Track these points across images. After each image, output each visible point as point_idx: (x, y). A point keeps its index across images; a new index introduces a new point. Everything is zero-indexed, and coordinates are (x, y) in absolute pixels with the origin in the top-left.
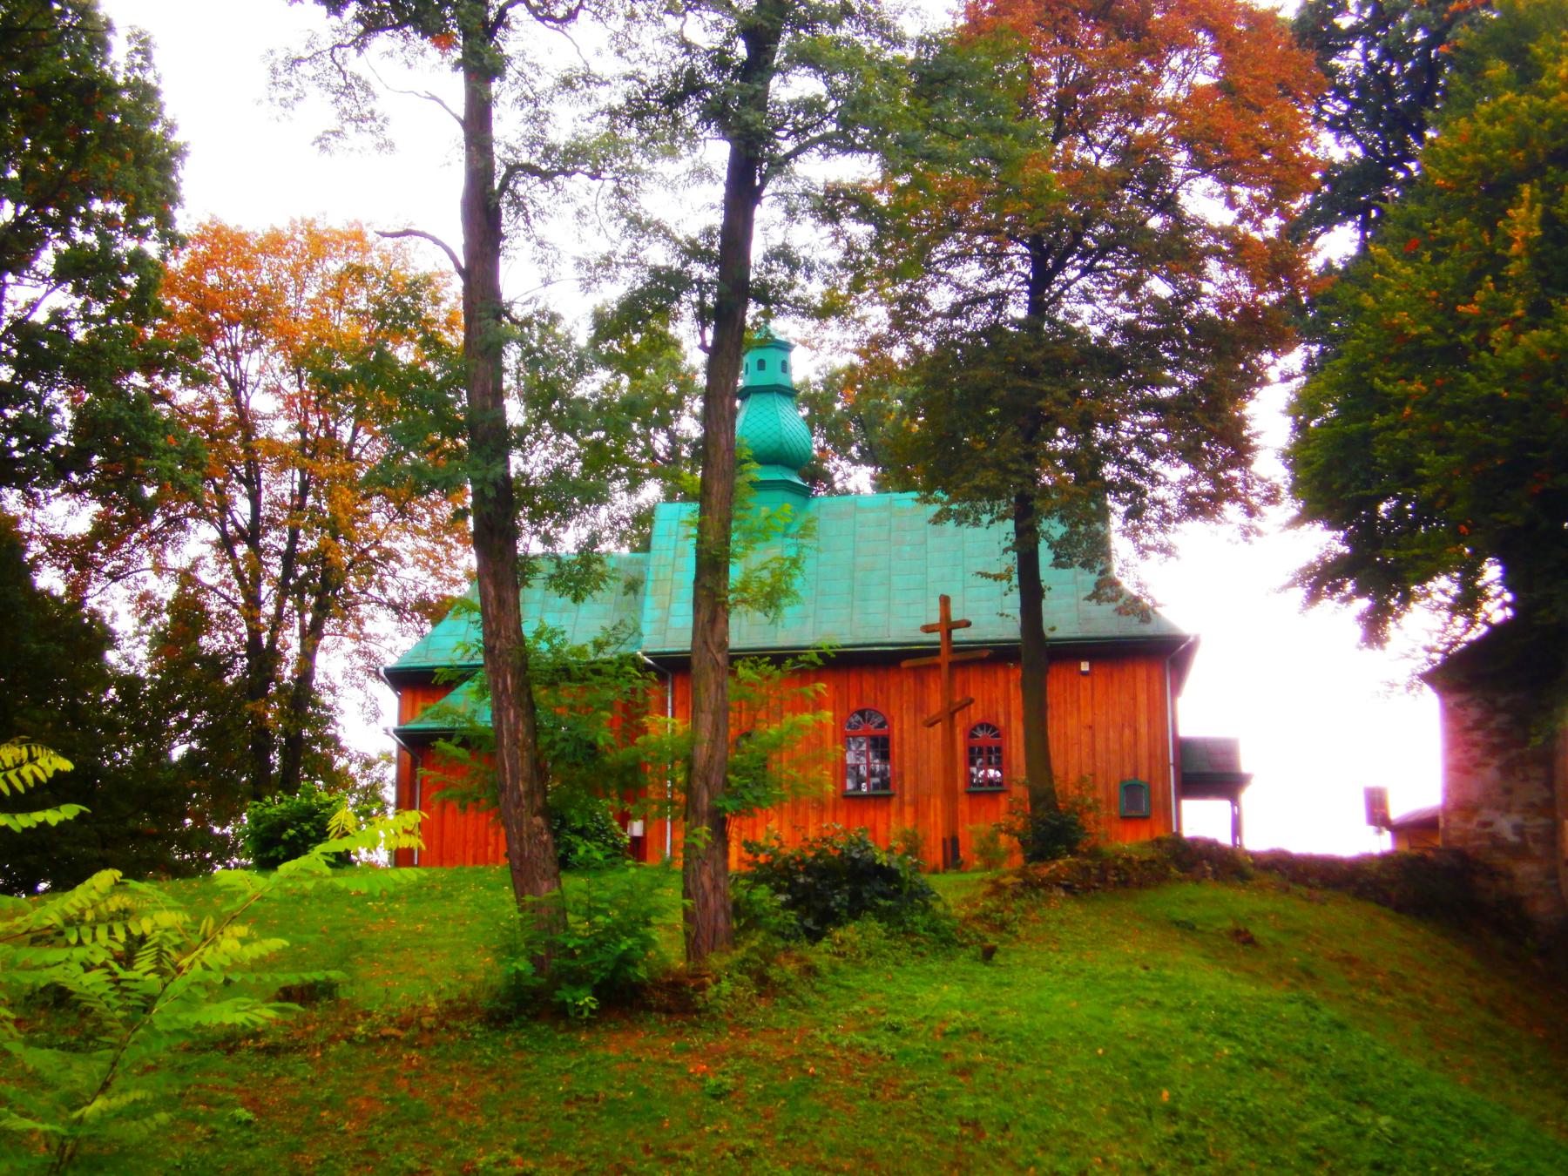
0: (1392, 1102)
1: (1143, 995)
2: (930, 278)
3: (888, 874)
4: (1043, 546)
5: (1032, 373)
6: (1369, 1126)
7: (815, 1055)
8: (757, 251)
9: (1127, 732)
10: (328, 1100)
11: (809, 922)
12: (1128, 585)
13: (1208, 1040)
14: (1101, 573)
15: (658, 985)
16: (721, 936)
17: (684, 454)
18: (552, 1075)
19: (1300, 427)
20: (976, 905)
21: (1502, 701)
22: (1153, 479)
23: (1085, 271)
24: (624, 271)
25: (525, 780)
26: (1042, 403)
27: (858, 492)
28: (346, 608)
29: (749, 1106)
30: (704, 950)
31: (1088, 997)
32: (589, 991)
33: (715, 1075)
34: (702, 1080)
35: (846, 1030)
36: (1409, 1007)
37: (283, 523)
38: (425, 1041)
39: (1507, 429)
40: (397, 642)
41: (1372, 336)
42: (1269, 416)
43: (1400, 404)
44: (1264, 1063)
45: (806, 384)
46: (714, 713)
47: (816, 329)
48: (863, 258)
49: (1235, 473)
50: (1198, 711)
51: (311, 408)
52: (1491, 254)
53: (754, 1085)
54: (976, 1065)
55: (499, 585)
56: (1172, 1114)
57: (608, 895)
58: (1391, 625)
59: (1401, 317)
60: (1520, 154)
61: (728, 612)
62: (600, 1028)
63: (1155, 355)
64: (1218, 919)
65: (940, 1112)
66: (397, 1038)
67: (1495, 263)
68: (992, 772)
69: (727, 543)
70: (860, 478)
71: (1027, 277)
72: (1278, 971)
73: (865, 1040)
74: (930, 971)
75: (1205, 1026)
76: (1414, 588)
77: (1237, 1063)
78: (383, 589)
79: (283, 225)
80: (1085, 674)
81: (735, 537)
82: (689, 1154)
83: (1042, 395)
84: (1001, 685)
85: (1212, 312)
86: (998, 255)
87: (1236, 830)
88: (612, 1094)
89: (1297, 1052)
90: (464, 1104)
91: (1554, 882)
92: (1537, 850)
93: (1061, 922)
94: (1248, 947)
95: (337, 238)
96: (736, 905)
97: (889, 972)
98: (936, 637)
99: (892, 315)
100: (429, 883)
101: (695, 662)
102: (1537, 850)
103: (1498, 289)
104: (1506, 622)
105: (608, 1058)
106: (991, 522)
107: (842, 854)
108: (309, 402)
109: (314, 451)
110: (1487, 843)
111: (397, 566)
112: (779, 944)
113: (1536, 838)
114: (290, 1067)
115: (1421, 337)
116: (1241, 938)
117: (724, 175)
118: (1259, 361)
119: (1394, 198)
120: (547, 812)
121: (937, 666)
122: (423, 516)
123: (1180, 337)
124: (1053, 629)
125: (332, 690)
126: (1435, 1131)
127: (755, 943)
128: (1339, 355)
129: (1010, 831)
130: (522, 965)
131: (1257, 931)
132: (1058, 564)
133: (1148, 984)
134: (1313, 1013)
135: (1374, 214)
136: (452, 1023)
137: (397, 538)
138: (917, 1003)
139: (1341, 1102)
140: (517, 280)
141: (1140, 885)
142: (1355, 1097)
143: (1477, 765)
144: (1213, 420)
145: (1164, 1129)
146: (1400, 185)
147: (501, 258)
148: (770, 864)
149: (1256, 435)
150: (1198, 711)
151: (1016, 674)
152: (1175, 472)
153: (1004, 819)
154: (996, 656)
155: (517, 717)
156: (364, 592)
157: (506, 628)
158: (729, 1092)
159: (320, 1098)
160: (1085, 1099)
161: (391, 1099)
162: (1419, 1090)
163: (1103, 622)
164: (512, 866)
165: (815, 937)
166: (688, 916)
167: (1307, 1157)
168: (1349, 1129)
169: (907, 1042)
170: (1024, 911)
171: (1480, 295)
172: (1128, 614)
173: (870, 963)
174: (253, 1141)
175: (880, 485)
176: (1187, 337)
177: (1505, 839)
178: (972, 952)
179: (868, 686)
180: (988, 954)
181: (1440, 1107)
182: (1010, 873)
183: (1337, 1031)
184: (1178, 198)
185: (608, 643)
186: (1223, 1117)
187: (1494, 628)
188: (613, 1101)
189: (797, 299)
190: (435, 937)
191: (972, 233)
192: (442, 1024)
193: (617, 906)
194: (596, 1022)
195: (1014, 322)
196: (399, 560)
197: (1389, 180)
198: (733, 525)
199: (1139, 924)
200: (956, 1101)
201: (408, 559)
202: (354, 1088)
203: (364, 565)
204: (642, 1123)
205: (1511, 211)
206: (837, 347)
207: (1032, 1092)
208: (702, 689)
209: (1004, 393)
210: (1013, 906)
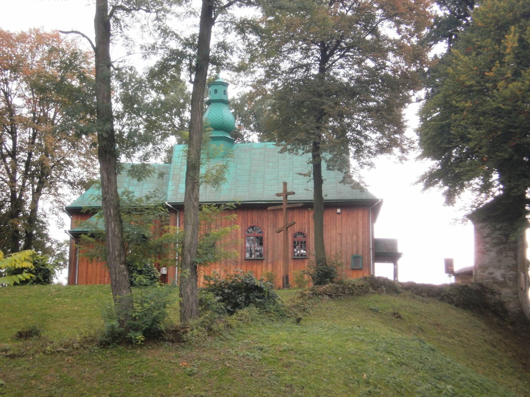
0: (452, 380)
2: (281, 58)
3: (259, 289)
5: (320, 96)
6: (443, 389)
7: (229, 359)
8: (213, 42)
9: (354, 236)
10: (34, 376)
11: (229, 308)
12: (355, 178)
14: (345, 173)
15: (168, 331)
16: (194, 312)
17: (186, 126)
18: (125, 367)
19: (422, 120)
20: (294, 302)
21: (498, 226)
22: (366, 138)
23: (341, 56)
24: (160, 51)
25: (118, 250)
26: (323, 107)
27: (253, 142)
28: (51, 183)
29: (203, 379)
30: (187, 318)
31: (336, 338)
32: (142, 334)
33: (190, 366)
34: (185, 369)
35: (242, 349)
36: (460, 343)
37: (26, 149)
38: (75, 353)
39: (503, 121)
40: (70, 197)
41: (451, 84)
42: (412, 115)
43: (462, 111)
44: (403, 364)
45: (233, 99)
47: (236, 77)
48: (254, 48)
49: (397, 136)
50: (382, 229)
51: (38, 103)
53: (205, 371)
54: (292, 363)
55: (108, 173)
56: (367, 383)
57: (149, 296)
58: (456, 197)
59: (463, 78)
60: (511, 14)
61: (199, 186)
62: (145, 347)
63: (367, 90)
64: (387, 308)
65: (278, 382)
66: (63, 352)
67: (500, 56)
68: (302, 251)
69: (199, 159)
70: (254, 137)
71: (319, 58)
73: (249, 353)
74: (276, 327)
75: (381, 349)
76: (466, 182)
77: (393, 363)
78: (66, 176)
79: (26, 30)
80: (339, 213)
81: (202, 156)
83: (323, 104)
84: (306, 217)
85: (390, 73)
86: (308, 49)
87: (396, 275)
88: (149, 374)
89: (416, 360)
90: (89, 378)
91: (516, 296)
92: (510, 284)
93: (327, 309)
94: (399, 319)
95: (48, 36)
96: (201, 300)
97: (259, 327)
98: (281, 198)
99: (267, 72)
101: (186, 205)
102: (510, 284)
103: (501, 66)
104: (500, 195)
105: (148, 360)
106: (303, 153)
107: (243, 281)
108: (36, 101)
109: (38, 121)
110: (491, 281)
111: (72, 167)
112: (217, 316)
113: (510, 279)
114: (20, 363)
115: (471, 86)
116: (396, 316)
117: (200, 14)
118: (408, 94)
119: (462, 31)
120: (126, 263)
121: (281, 209)
122: (82, 148)
123: (378, 83)
124: (326, 196)
125: (45, 216)
126: (469, 391)
127: (207, 315)
128: (439, 92)
129: (308, 273)
130: (115, 323)
131: (402, 313)
132: (328, 168)
134: (423, 345)
135: (453, 37)
136: (86, 346)
137: (72, 156)
138: (270, 339)
139: (433, 379)
140: (116, 52)
142: (438, 378)
143: (487, 251)
144: (389, 115)
145: (364, 389)
146: (464, 26)
147: (111, 44)
148: (215, 285)
149: (406, 121)
150: (382, 229)
151: (311, 214)
152: (374, 136)
153: (306, 269)
154: (306, 206)
155: (115, 225)
156: (58, 177)
157: (111, 191)
158: (195, 373)
159: (31, 375)
160: (334, 377)
161: (60, 376)
162: (463, 375)
163: (346, 193)
164: (112, 285)
165: (231, 313)
166: (181, 304)
168: (435, 390)
169: (265, 354)
170: (313, 304)
171: (494, 69)
172: (356, 189)
173: (252, 323)
174: (3, 392)
175: (261, 140)
176: (380, 83)
177: (498, 279)
178: (293, 320)
179: (254, 217)
180: (299, 320)
181: (471, 382)
182: (308, 289)
183: (432, 352)
184: (378, 28)
185: (151, 197)
187: (496, 198)
188: (149, 377)
189: (228, 64)
190: (82, 312)
191: (297, 40)
192: (82, 346)
193: (153, 300)
194: (143, 345)
195: (313, 75)
196: (73, 165)
197: (460, 24)
198: (202, 151)
199: (357, 310)
200: (284, 377)
201: (76, 165)
202: (45, 372)
203: (59, 166)
204: (160, 385)
205: (506, 36)
206: (245, 84)
207: (313, 374)
208: (188, 216)
209: (308, 103)
210: (308, 302)
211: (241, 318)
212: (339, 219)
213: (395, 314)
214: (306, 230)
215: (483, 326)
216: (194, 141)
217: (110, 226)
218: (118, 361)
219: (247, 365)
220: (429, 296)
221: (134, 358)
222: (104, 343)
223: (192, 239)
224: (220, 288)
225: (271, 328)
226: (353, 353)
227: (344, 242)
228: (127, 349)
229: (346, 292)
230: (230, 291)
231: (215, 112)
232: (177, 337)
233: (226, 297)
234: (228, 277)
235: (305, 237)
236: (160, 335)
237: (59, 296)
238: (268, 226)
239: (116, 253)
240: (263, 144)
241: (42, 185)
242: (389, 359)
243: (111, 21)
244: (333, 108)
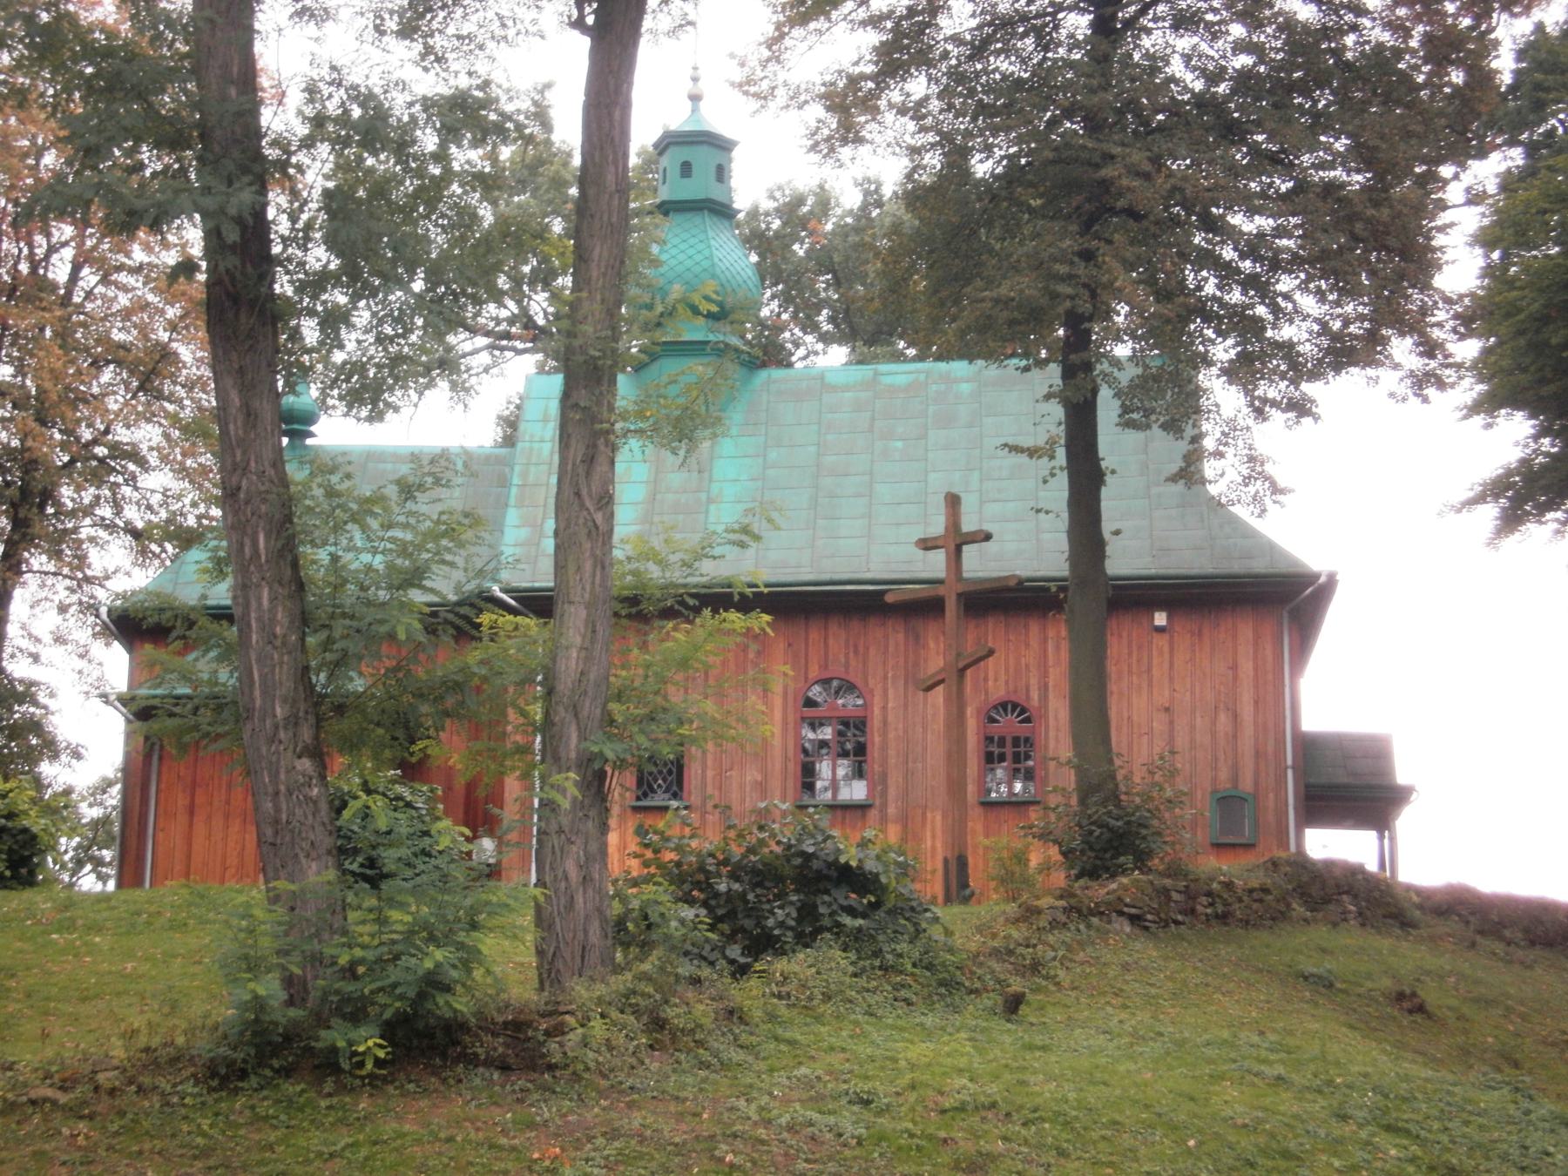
1: (1256, 1067)
4: (1105, 394)
7: (735, 1136)
9: (1223, 718)
13: (1363, 1134)
18: (307, 1162)
25: (284, 701)
26: (1108, 172)
31: (1171, 1068)
32: (377, 1031)
35: (786, 1101)
40: (122, 572)
46: (588, 606)
50: (1330, 695)
54: (992, 1157)
61: (614, 449)
62: (390, 1089)
64: (1369, 976)
66: (54, 1103)
72: (1466, 1055)
73: (815, 1116)
74: (921, 1024)
75: (1360, 1114)
89: (1505, 1158)
93: (1126, 967)
94: (1418, 1018)
97: (856, 1023)
98: (935, 564)
100: (153, 909)
105: (402, 1135)
112: (686, 969)
116: (1406, 1005)
127: (646, 966)
131: (1430, 995)
133: (1264, 1053)
134: (1526, 1104)
136: (146, 1080)
141: (1246, 923)
150: (1330, 695)
163: (1186, 556)
165: (740, 971)
166: (541, 920)
170: (1069, 949)
173: (828, 1009)
178: (989, 1003)
179: (834, 643)
180: (1013, 1005)
185: (421, 487)
194: (385, 1080)
196: (142, 463)
199: (1246, 974)
201: (153, 459)
211: (784, 989)
212: (1161, 653)
213: (1401, 997)
214: (1035, 695)
216: (594, 265)
217: (254, 604)
218: (279, 1142)
219: (807, 1161)
220: (1533, 943)
221: (344, 1130)
222: (223, 1071)
223: (587, 659)
224: (701, 877)
225: (902, 1029)
226: (1245, 1126)
228: (319, 1093)
229: (1199, 908)
230: (736, 886)
231: (683, 246)
232: (520, 1048)
233: (720, 912)
234: (732, 834)
235: (1028, 720)
236: (456, 1043)
237: (68, 926)
238: (885, 678)
239: (278, 711)
240: (866, 371)
241: (24, 535)
242: (1393, 1152)
244: (1147, 176)
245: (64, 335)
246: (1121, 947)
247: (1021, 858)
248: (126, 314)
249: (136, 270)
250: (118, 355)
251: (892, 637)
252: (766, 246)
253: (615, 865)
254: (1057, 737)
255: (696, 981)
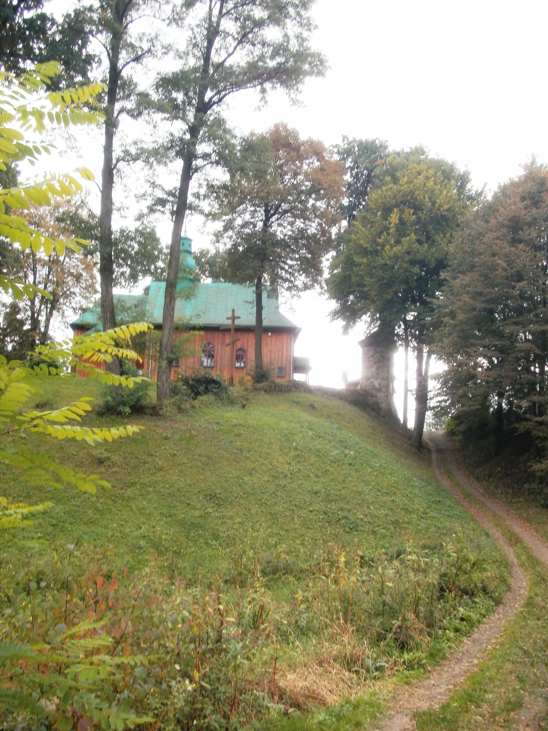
3: (214, 382)
8: (190, 192)
9: (280, 353)
21: (378, 350)
43: (361, 265)
44: (320, 437)
50: (300, 349)
52: (385, 227)
53: (177, 437)
56: (296, 449)
59: (362, 242)
61: (175, 300)
72: (321, 416)
78: (71, 303)
82: (157, 454)
92: (384, 390)
98: (230, 322)
112: (185, 398)
115: (367, 248)
130: (109, 398)
163: (275, 323)
165: (194, 399)
167: (331, 461)
171: (382, 237)
173: (210, 406)
180: (244, 406)
186: (310, 450)
201: (78, 295)
215: (367, 417)
227: (273, 357)
243: (114, 172)
245: (62, 270)
246: (263, 396)
247: (243, 378)
248: (74, 267)
249: (76, 258)
250: (71, 274)
251: (220, 335)
252: (197, 259)
253: (172, 378)
254: (251, 355)
255: (186, 400)
